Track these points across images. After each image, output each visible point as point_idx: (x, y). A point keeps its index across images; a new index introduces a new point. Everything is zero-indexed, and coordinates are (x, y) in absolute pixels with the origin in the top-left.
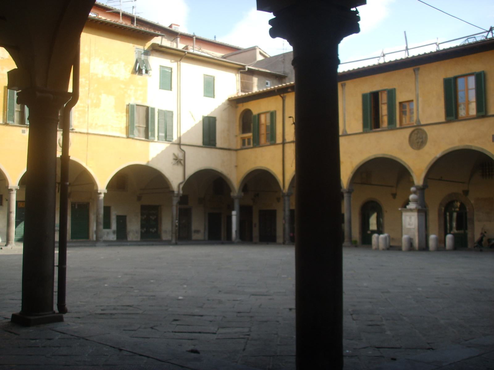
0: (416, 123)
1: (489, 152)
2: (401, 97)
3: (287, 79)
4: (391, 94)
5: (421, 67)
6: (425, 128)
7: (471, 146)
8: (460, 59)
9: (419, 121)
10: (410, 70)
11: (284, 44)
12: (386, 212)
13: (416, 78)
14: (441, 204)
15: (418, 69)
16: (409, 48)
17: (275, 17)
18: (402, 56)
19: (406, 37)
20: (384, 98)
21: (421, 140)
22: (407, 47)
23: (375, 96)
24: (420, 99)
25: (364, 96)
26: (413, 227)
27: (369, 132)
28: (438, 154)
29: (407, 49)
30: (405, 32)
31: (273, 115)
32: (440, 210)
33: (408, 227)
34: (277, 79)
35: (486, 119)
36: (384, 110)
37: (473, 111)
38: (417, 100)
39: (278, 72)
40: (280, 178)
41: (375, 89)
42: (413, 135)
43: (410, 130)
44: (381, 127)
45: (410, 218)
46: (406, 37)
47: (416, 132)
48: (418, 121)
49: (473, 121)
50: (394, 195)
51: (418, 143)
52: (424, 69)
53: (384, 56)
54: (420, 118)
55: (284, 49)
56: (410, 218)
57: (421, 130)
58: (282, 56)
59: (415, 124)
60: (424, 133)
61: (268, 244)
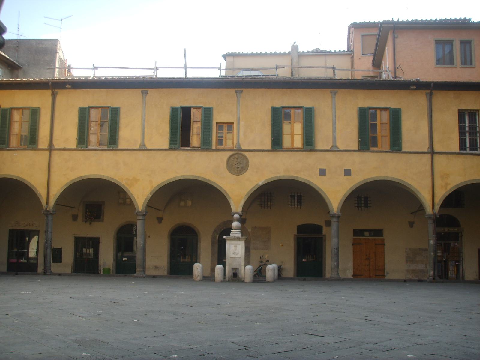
0: (235, 147)
1: (316, 185)
2: (218, 117)
3: (20, 73)
4: (208, 113)
5: (245, 90)
6: (246, 154)
7: (298, 177)
8: (289, 91)
9: (239, 146)
10: (232, 91)
11: (18, 28)
12: (149, 237)
13: (238, 102)
14: (215, 231)
15: (242, 92)
16: (187, 66)
17: (471, 21)
18: (178, 74)
19: (185, 55)
20: (197, 115)
21: (241, 166)
22: (185, 65)
23: (186, 112)
24: (242, 123)
25: (174, 110)
26: (239, 256)
27: (176, 150)
28: (261, 182)
29: (185, 67)
30: (185, 49)
31: (35, 113)
32: (213, 238)
33: (234, 256)
34: (9, 69)
35: (313, 153)
36: (196, 128)
37: (298, 142)
38: (239, 124)
39: (17, 62)
40: (42, 192)
41: (186, 104)
42: (232, 158)
43: (231, 153)
44: (191, 146)
45: (236, 247)
46: (185, 55)
47: (236, 156)
48: (239, 145)
49: (300, 153)
50: (160, 220)
51: (238, 168)
52: (248, 93)
53: (95, 68)
54: (240, 142)
55: (18, 34)
56: (236, 247)
57: (242, 154)
58: (16, 42)
59: (235, 148)
60: (246, 158)
61: (17, 274)
